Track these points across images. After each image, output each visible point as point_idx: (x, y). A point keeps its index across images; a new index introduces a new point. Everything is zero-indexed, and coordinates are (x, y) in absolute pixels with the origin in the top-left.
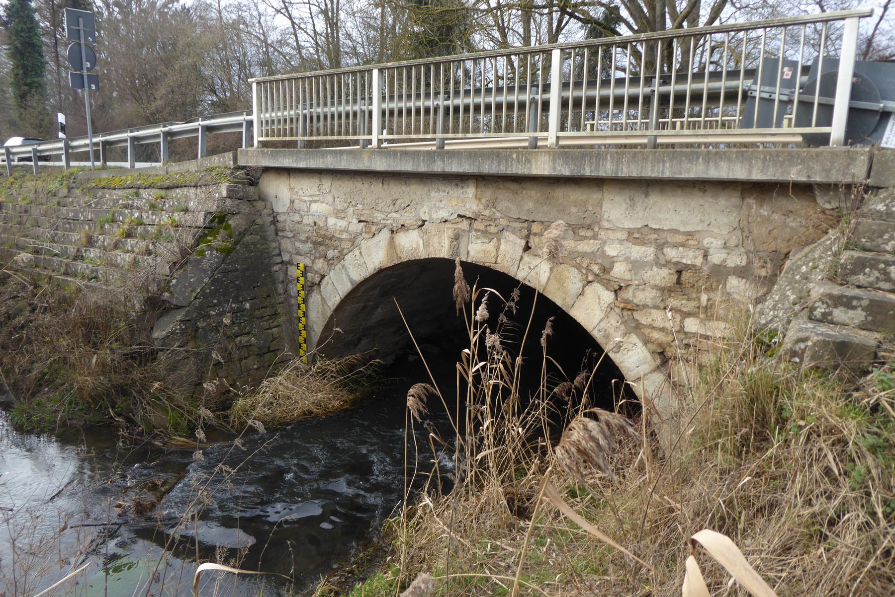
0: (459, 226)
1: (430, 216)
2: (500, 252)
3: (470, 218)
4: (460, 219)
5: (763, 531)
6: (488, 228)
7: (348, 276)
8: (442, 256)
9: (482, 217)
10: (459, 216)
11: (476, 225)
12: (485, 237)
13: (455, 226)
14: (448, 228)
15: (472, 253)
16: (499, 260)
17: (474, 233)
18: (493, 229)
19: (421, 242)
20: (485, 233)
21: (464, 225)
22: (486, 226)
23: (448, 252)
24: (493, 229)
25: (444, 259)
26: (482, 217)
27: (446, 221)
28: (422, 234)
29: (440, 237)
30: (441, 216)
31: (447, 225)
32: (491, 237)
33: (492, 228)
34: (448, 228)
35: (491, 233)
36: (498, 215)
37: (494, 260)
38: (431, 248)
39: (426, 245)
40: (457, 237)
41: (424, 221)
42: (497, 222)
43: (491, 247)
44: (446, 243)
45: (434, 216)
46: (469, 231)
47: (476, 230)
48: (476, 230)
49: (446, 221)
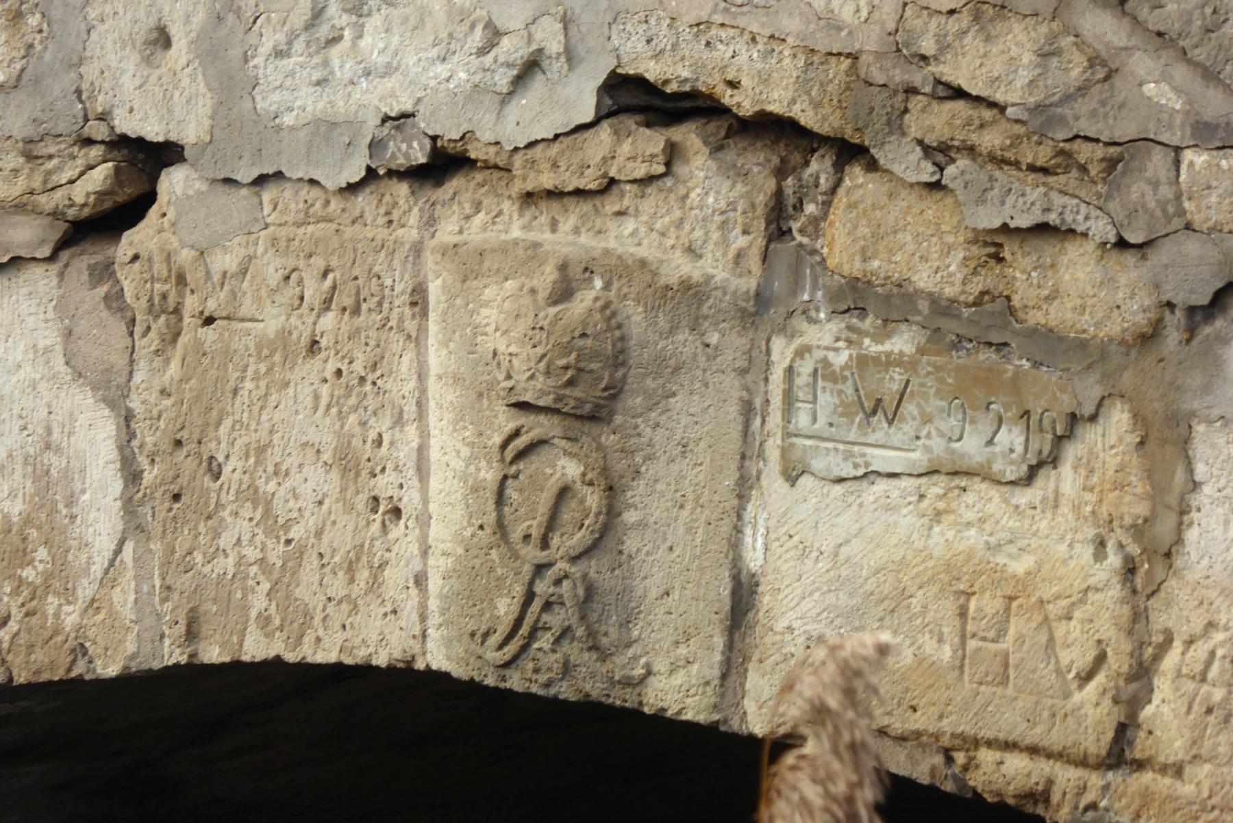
0: (633, 233)
1: (232, 84)
2: (1177, 611)
3: (771, 128)
4: (640, 146)
5: (1208, 219)
6: (1023, 276)
7: (1057, 487)
8: (377, 639)
9: (938, 120)
10: (633, 98)
11: (861, 225)
12: (972, 394)
13: (567, 235)
14: (470, 265)
15: (794, 613)
16: (1164, 712)
17: (824, 334)
18: (1081, 290)
19: (95, 440)
20: (979, 333)
21: (699, 218)
22: (994, 244)
23: (471, 586)
24: (1081, 290)
25: (406, 685)
26: (938, 120)
27: (444, 164)
28: (105, 338)
29: (360, 384)
30: (377, 98)
31: (467, 218)
32: (1054, 392)
33: (1078, 268)
34: (470, 265)
35: (1052, 346)
36: (1159, 90)
37: (1090, 713)
38: (238, 527)
39: (169, 482)
40: (586, 392)
41: (146, 160)
42: (1143, 190)
43: (1051, 537)
44: (445, 465)
45: (291, 93)
46: (758, 311)
47: (855, 298)
48: (855, 298)
49: (444, 164)
